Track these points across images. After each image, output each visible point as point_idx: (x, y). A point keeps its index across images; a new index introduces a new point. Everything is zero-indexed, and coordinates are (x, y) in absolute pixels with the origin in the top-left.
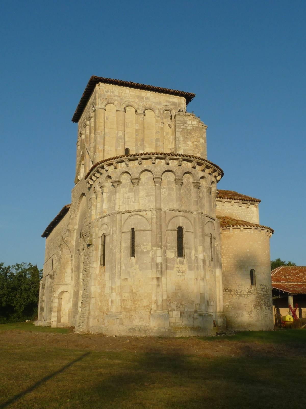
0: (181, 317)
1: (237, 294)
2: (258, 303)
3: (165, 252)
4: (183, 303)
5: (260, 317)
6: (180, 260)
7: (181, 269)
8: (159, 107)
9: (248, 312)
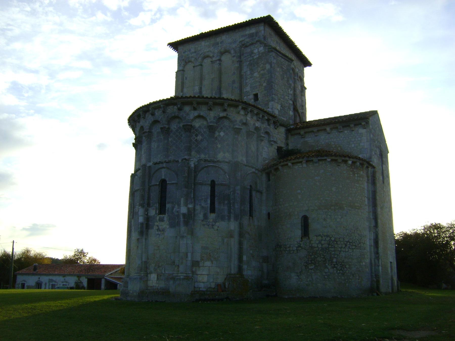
0: (157, 280)
2: (311, 261)
3: (147, 210)
4: (160, 265)
6: (160, 217)
7: (160, 227)
8: (234, 46)
9: (297, 273)
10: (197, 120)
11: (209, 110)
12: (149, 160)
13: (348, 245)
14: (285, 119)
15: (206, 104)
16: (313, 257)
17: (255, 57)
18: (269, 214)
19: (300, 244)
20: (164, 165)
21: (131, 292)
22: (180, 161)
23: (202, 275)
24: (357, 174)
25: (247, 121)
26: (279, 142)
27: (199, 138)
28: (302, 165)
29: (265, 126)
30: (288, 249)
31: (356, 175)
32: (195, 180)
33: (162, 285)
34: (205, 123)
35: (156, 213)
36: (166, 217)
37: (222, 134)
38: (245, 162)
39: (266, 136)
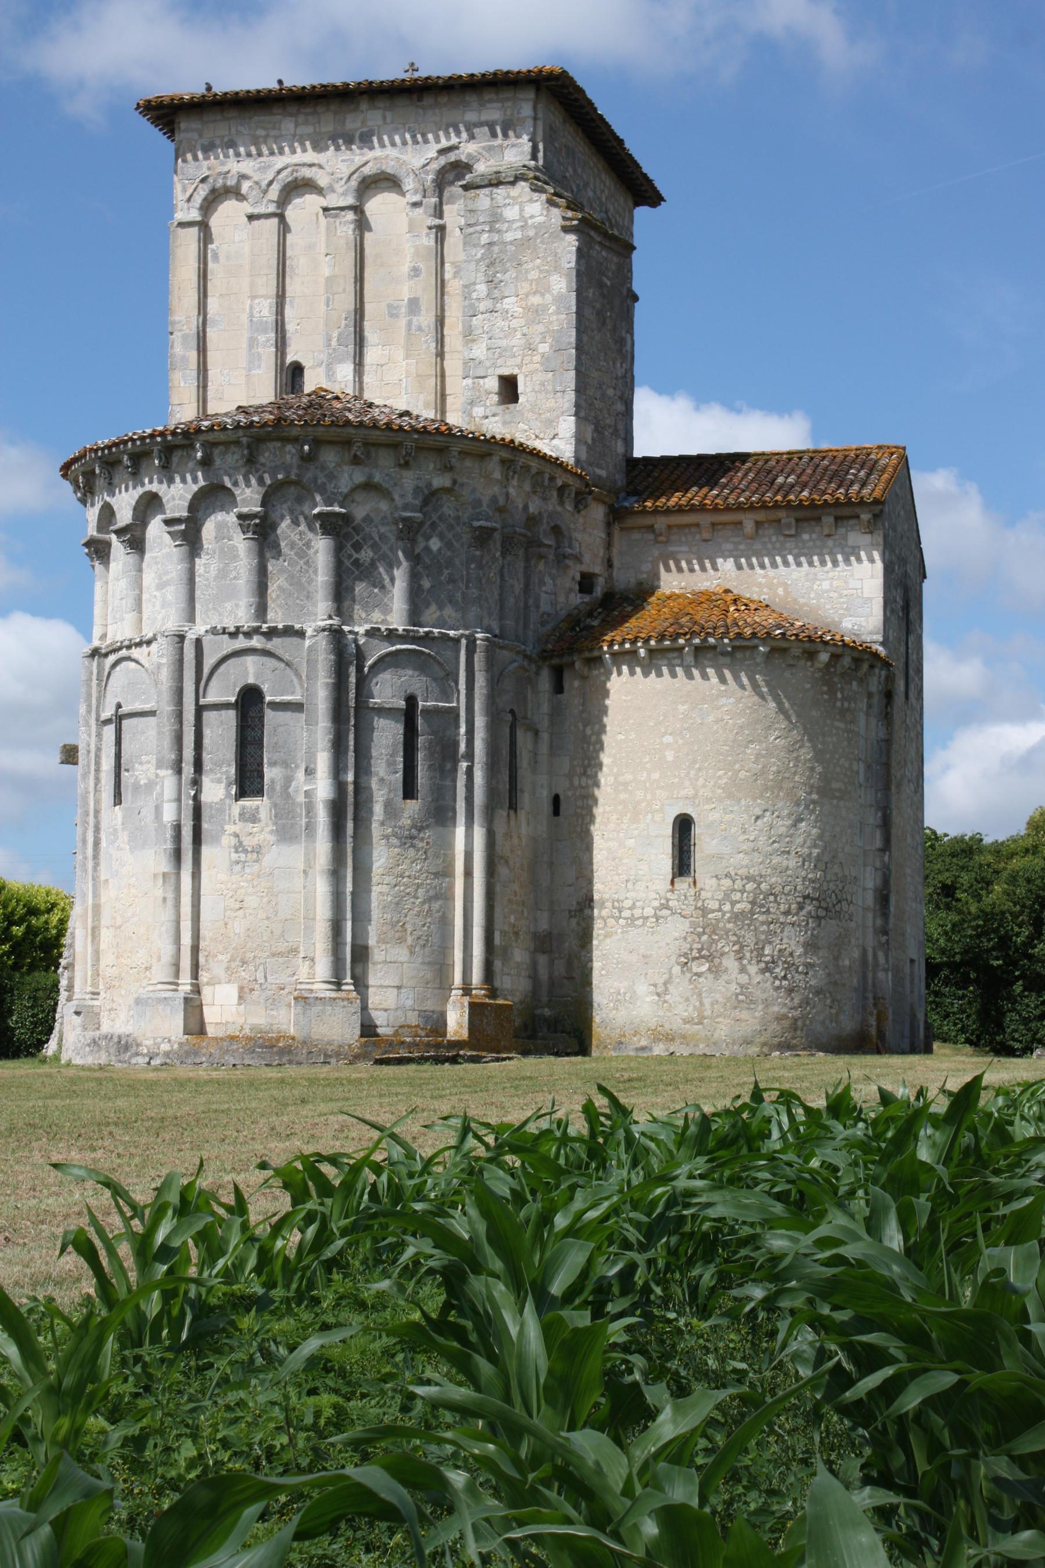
0: (239, 1004)
5: (707, 1002)
7: (247, 842)
9: (655, 985)
10: (359, 497)
11: (400, 465)
14: (603, 473)
16: (705, 938)
17: (509, 237)
18: (556, 801)
19: (668, 900)
20: (256, 642)
22: (309, 632)
24: (842, 690)
26: (587, 558)
27: (366, 555)
29: (551, 508)
30: (626, 913)
31: (839, 695)
33: (256, 1018)
34: (384, 506)
35: (228, 795)
37: (435, 544)
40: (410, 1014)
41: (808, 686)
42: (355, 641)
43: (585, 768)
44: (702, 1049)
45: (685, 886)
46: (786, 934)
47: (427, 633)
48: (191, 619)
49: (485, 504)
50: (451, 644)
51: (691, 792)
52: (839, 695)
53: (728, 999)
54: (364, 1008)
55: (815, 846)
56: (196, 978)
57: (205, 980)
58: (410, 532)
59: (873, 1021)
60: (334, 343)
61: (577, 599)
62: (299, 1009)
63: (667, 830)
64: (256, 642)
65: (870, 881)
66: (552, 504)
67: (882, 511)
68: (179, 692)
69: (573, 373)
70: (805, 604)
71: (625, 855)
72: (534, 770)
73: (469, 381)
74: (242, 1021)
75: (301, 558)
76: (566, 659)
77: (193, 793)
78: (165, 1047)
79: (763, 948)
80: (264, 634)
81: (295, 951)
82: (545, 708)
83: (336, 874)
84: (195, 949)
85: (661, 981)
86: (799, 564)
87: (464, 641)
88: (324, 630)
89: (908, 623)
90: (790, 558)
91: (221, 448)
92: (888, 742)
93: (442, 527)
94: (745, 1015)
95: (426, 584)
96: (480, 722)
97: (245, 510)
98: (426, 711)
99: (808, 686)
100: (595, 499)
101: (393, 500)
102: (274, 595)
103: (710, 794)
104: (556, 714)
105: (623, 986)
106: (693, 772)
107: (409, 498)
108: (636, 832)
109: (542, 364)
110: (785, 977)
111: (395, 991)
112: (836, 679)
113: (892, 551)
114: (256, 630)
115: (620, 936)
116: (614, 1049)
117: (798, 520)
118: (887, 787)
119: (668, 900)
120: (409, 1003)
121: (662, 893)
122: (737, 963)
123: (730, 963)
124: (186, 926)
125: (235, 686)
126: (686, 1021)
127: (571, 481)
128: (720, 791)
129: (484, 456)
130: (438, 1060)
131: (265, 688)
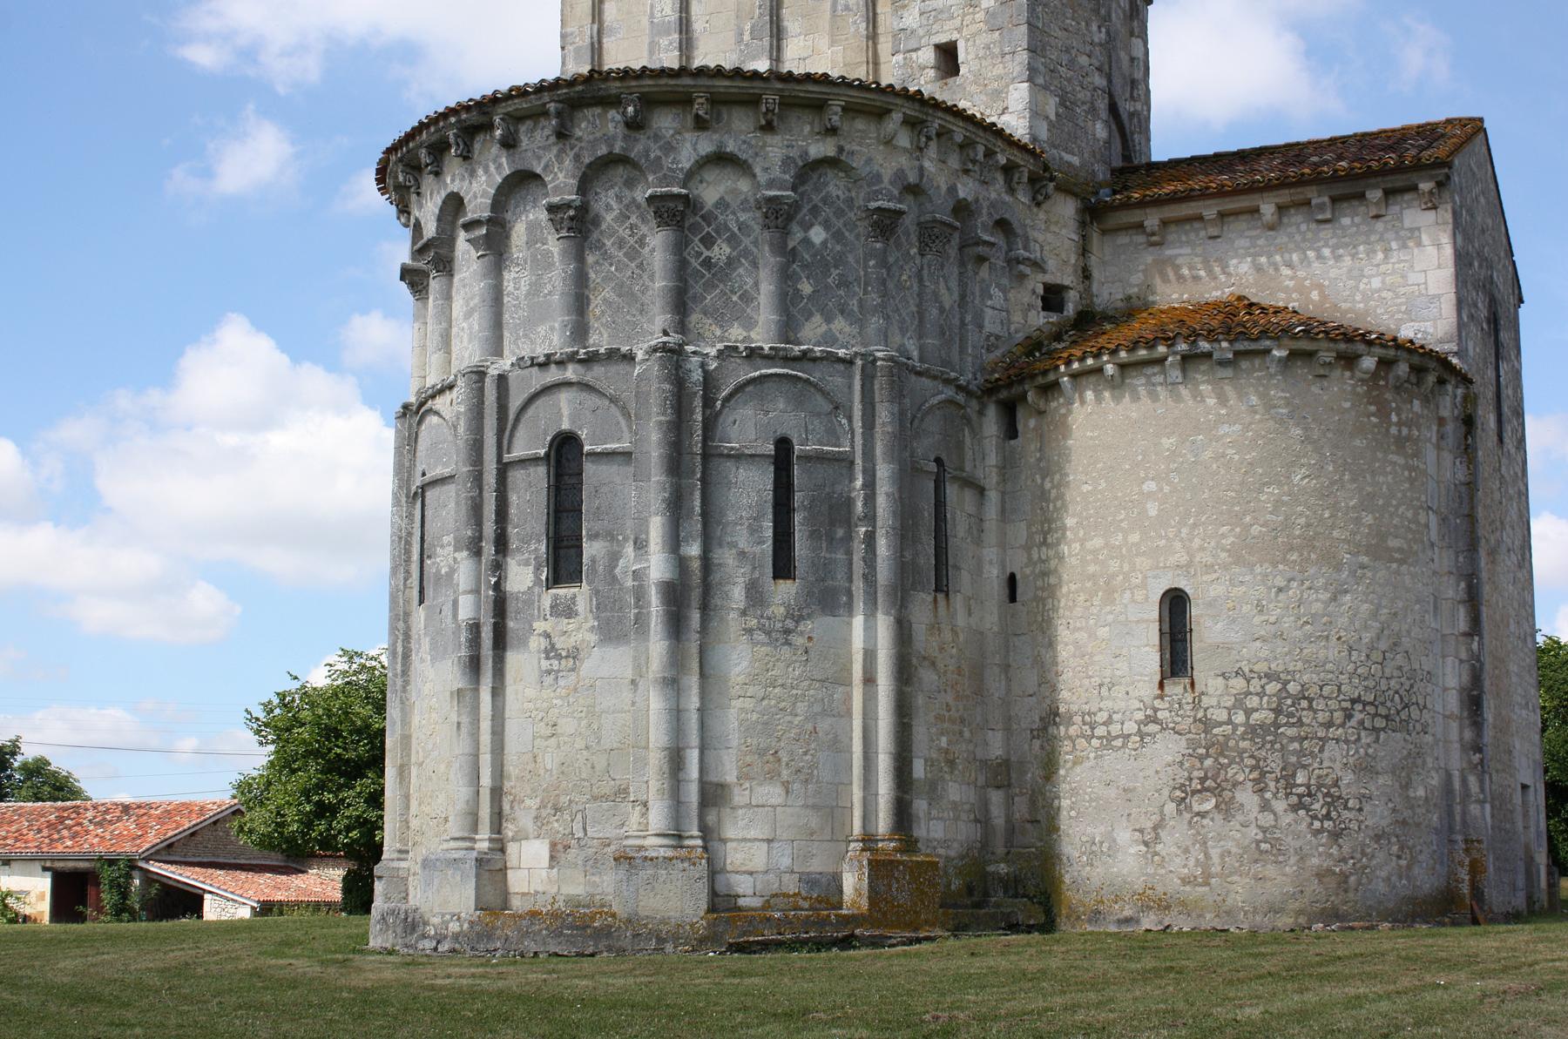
0: (551, 867)
1: (1093, 736)
4: (564, 800)
5: (1215, 853)
6: (556, 597)
7: (560, 643)
9: (1141, 831)
10: (710, 175)
11: (762, 128)
12: (496, 346)
13: (1358, 716)
14: (1075, 160)
15: (752, 102)
16: (1209, 762)
18: (1012, 580)
19: (1156, 710)
20: (571, 373)
21: (436, 920)
22: (640, 355)
23: (744, 840)
24: (1399, 412)
25: (921, 175)
26: (1051, 264)
27: (721, 251)
28: (1164, 372)
29: (993, 195)
31: (1394, 418)
32: (706, 438)
33: (574, 886)
34: (744, 185)
35: (537, 581)
36: (580, 595)
37: (818, 235)
38: (915, 354)
39: (998, 239)
40: (786, 878)
41: (1347, 405)
42: (703, 365)
43: (1045, 534)
44: (1209, 921)
45: (1179, 689)
46: (1326, 754)
47: (804, 353)
48: (498, 352)
49: (886, 180)
50: (841, 367)
51: (1184, 559)
52: (1394, 418)
53: (1246, 849)
54: (714, 871)
55: (1366, 627)
56: (499, 832)
57: (510, 834)
58: (779, 217)
59: (1464, 875)
60: (747, 37)
61: (1040, 319)
62: (622, 873)
63: (1150, 613)
64: (571, 373)
65: (1453, 677)
66: (997, 190)
67: (1448, 177)
68: (477, 447)
69: (1024, 28)
70: (1347, 311)
71: (1100, 652)
72: (979, 542)
73: (900, 57)
74: (555, 890)
75: (632, 259)
76: (1016, 390)
77: (493, 580)
78: (454, 927)
79: (1294, 775)
80: (581, 361)
81: (622, 792)
82: (992, 459)
83: (672, 683)
84: (497, 793)
85: (1149, 825)
86: (1338, 258)
87: (859, 362)
88: (655, 350)
89: (1497, 344)
90: (1326, 252)
91: (529, 123)
92: (1471, 486)
93: (827, 212)
94: (1271, 871)
95: (806, 288)
96: (884, 471)
97: (556, 199)
98: (806, 458)
99: (1347, 405)
100: (1058, 189)
101: (754, 176)
102: (597, 311)
103: (1210, 560)
104: (1008, 466)
105: (1098, 832)
106: (1185, 531)
107: (777, 172)
108: (1110, 618)
109: (986, 22)
110: (1328, 816)
111: (765, 846)
112: (1388, 396)
113: (1468, 238)
114: (572, 358)
115: (1092, 763)
116: (1090, 921)
117: (1335, 200)
118: (1473, 546)
119: (1156, 710)
120: (786, 862)
121: (1148, 701)
122: (1256, 798)
123: (1247, 797)
124: (486, 759)
125: (546, 434)
126: (1185, 881)
127: (1019, 158)
128: (1224, 555)
129: (881, 114)
130: (819, 945)
131: (583, 434)
